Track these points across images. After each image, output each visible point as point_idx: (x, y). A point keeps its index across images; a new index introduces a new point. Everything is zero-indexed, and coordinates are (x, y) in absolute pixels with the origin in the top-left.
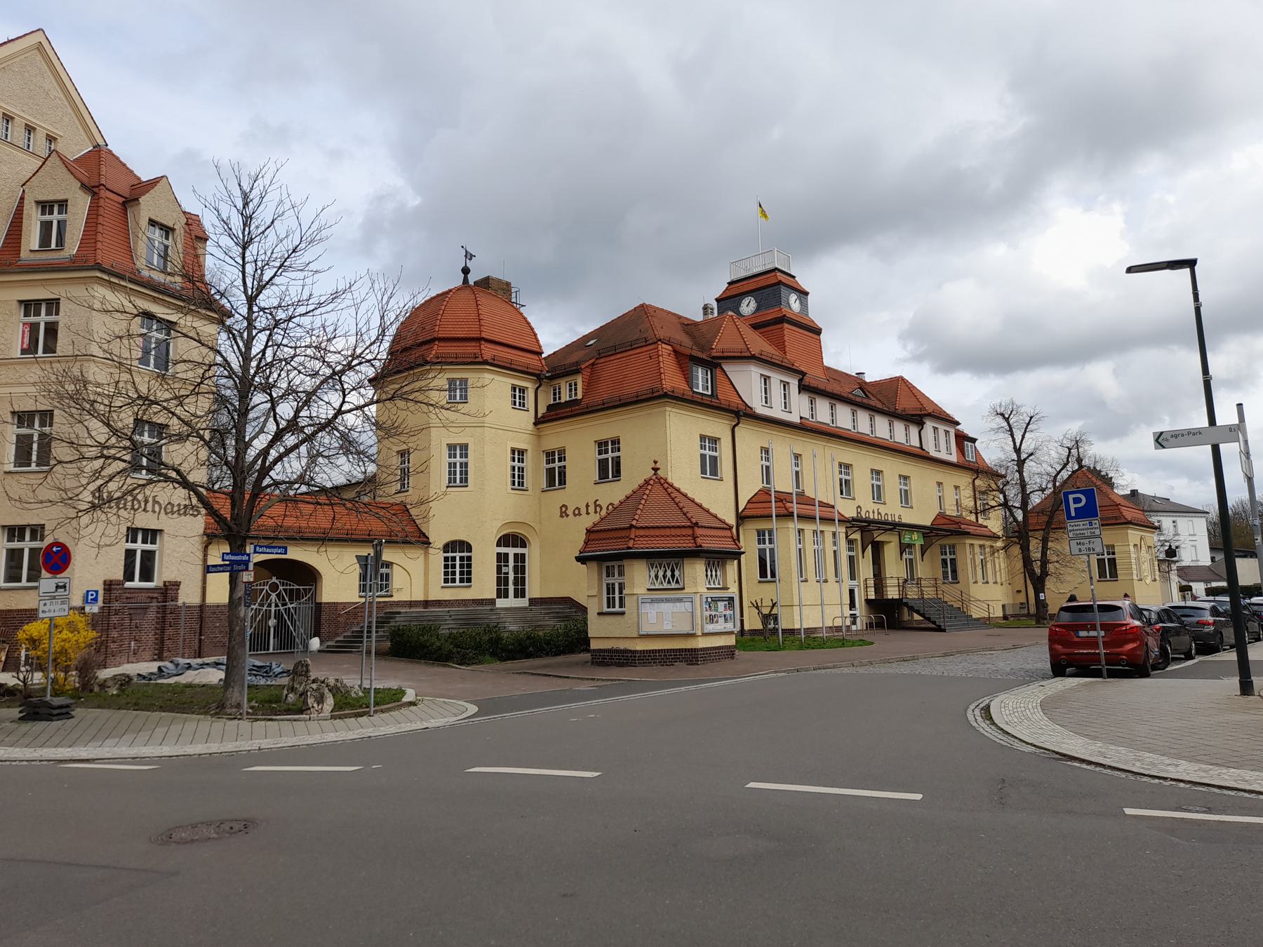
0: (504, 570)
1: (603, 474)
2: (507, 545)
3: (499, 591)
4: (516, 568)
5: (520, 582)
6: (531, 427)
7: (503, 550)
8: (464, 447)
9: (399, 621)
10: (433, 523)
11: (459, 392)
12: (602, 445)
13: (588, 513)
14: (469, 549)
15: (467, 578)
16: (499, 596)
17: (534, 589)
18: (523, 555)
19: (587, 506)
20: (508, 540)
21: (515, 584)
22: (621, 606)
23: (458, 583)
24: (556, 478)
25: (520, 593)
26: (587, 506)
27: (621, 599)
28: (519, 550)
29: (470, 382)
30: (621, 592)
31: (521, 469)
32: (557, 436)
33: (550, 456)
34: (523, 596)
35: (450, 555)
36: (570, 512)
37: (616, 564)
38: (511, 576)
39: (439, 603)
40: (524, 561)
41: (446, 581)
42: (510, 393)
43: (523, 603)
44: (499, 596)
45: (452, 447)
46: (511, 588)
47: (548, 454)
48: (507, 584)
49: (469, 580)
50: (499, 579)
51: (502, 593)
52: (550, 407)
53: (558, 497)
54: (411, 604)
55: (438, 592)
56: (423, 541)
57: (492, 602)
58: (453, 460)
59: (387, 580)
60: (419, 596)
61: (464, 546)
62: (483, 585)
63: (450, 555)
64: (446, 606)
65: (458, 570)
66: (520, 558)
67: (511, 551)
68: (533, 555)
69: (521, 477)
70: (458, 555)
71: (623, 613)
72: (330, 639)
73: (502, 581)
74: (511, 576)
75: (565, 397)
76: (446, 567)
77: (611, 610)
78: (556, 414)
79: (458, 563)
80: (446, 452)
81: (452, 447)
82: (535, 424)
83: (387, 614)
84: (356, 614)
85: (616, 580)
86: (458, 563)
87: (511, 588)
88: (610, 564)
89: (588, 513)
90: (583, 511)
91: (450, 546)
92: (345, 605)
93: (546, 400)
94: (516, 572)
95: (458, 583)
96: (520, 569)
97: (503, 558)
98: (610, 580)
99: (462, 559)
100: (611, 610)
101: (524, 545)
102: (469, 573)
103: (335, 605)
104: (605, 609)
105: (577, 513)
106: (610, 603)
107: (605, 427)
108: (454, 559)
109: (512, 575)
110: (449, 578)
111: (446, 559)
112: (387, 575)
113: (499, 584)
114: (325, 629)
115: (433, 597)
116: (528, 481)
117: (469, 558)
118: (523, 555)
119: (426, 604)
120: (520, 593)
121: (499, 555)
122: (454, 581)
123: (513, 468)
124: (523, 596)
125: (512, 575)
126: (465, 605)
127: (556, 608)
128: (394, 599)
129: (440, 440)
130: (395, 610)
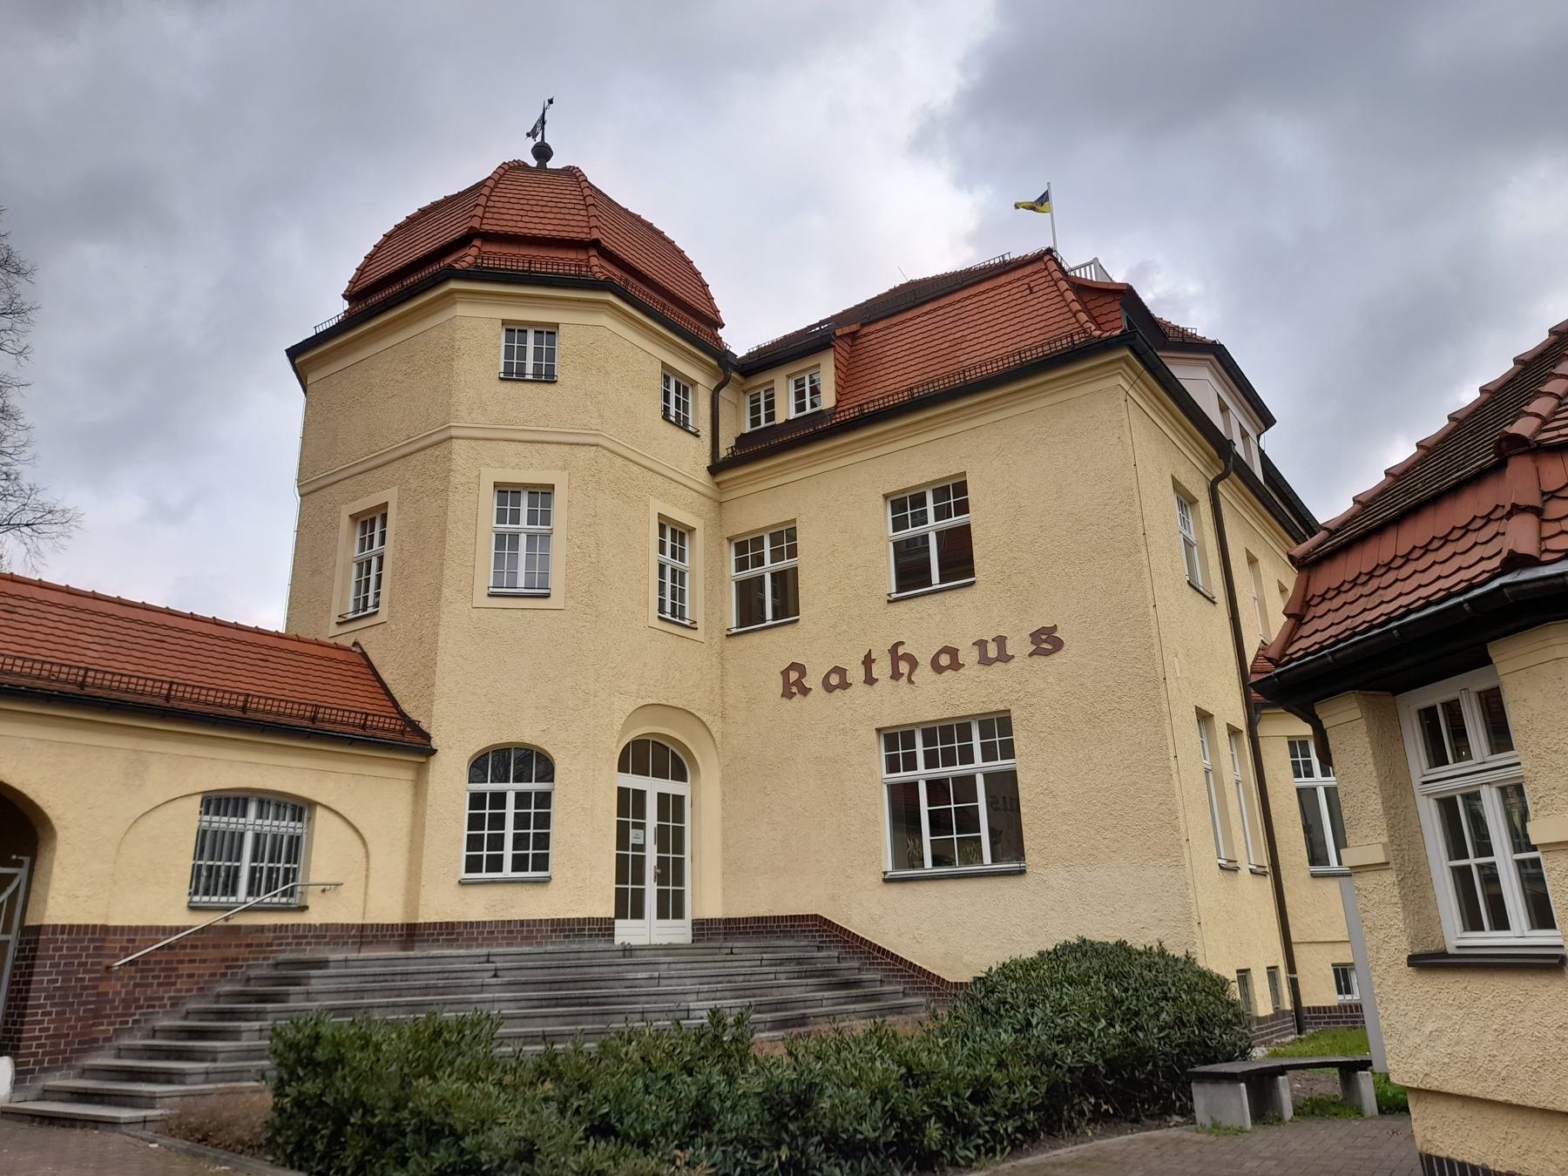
0: (634, 836)
1: (911, 574)
2: (641, 770)
3: (620, 895)
4: (661, 832)
5: (671, 872)
6: (704, 476)
7: (633, 781)
8: (542, 493)
9: (315, 999)
10: (439, 706)
11: (531, 361)
12: (905, 506)
13: (870, 680)
14: (547, 773)
15: (535, 856)
16: (621, 913)
17: (708, 897)
18: (679, 800)
19: (868, 661)
20: (646, 754)
21: (661, 878)
22: (1542, 915)
23: (507, 871)
24: (768, 599)
25: (671, 906)
26: (868, 661)
27: (1532, 876)
28: (671, 787)
29: (563, 343)
30: (1520, 840)
31: (678, 576)
32: (765, 500)
33: (747, 550)
34: (679, 914)
35: (489, 787)
36: (813, 681)
37: (1463, 689)
38: (651, 856)
39: (449, 932)
40: (679, 817)
41: (473, 865)
42: (659, 385)
43: (677, 932)
44: (621, 913)
45: (506, 492)
46: (651, 889)
47: (741, 548)
48: (639, 878)
49: (542, 863)
50: (621, 861)
51: (628, 904)
52: (742, 440)
53: (774, 647)
54: (365, 935)
55: (449, 898)
56: (409, 742)
57: (604, 928)
58: (508, 527)
59: (293, 855)
60: (388, 910)
61: (528, 762)
62: (579, 882)
63: (489, 787)
64: (471, 941)
65: (509, 831)
66: (671, 807)
67: (653, 786)
68: (705, 798)
69: (678, 594)
70: (511, 788)
71: (1547, 964)
72: (59, 1060)
73: (628, 868)
74: (651, 856)
75: (786, 410)
76: (475, 821)
77: (1489, 938)
78: (762, 446)
79: (510, 811)
80: (489, 503)
81: (506, 492)
82: (716, 468)
83: (287, 960)
84: (170, 969)
85: (1477, 771)
86: (510, 811)
87: (651, 889)
88: (1435, 695)
89: (870, 680)
90: (856, 674)
91: (498, 761)
92: (134, 935)
93: (737, 423)
94: (662, 846)
95: (507, 871)
96: (672, 839)
97: (630, 803)
98: (1454, 777)
99: (522, 799)
100: (1489, 938)
101: (680, 775)
102: (543, 841)
103: (100, 934)
104: (1455, 936)
105: (837, 681)
106: (1479, 901)
107: (915, 458)
108: (499, 799)
109: (651, 860)
110: (481, 857)
111: (477, 800)
112: (295, 841)
113: (621, 877)
114: (41, 1024)
115: (427, 915)
116: (695, 606)
117: (545, 799)
118: (679, 800)
119: (411, 934)
120: (671, 906)
121: (623, 792)
122: (495, 864)
123: (662, 567)
124: (679, 914)
125: (651, 860)
126: (528, 939)
127: (792, 947)
128: (314, 917)
129: (476, 475)
130: (308, 954)
